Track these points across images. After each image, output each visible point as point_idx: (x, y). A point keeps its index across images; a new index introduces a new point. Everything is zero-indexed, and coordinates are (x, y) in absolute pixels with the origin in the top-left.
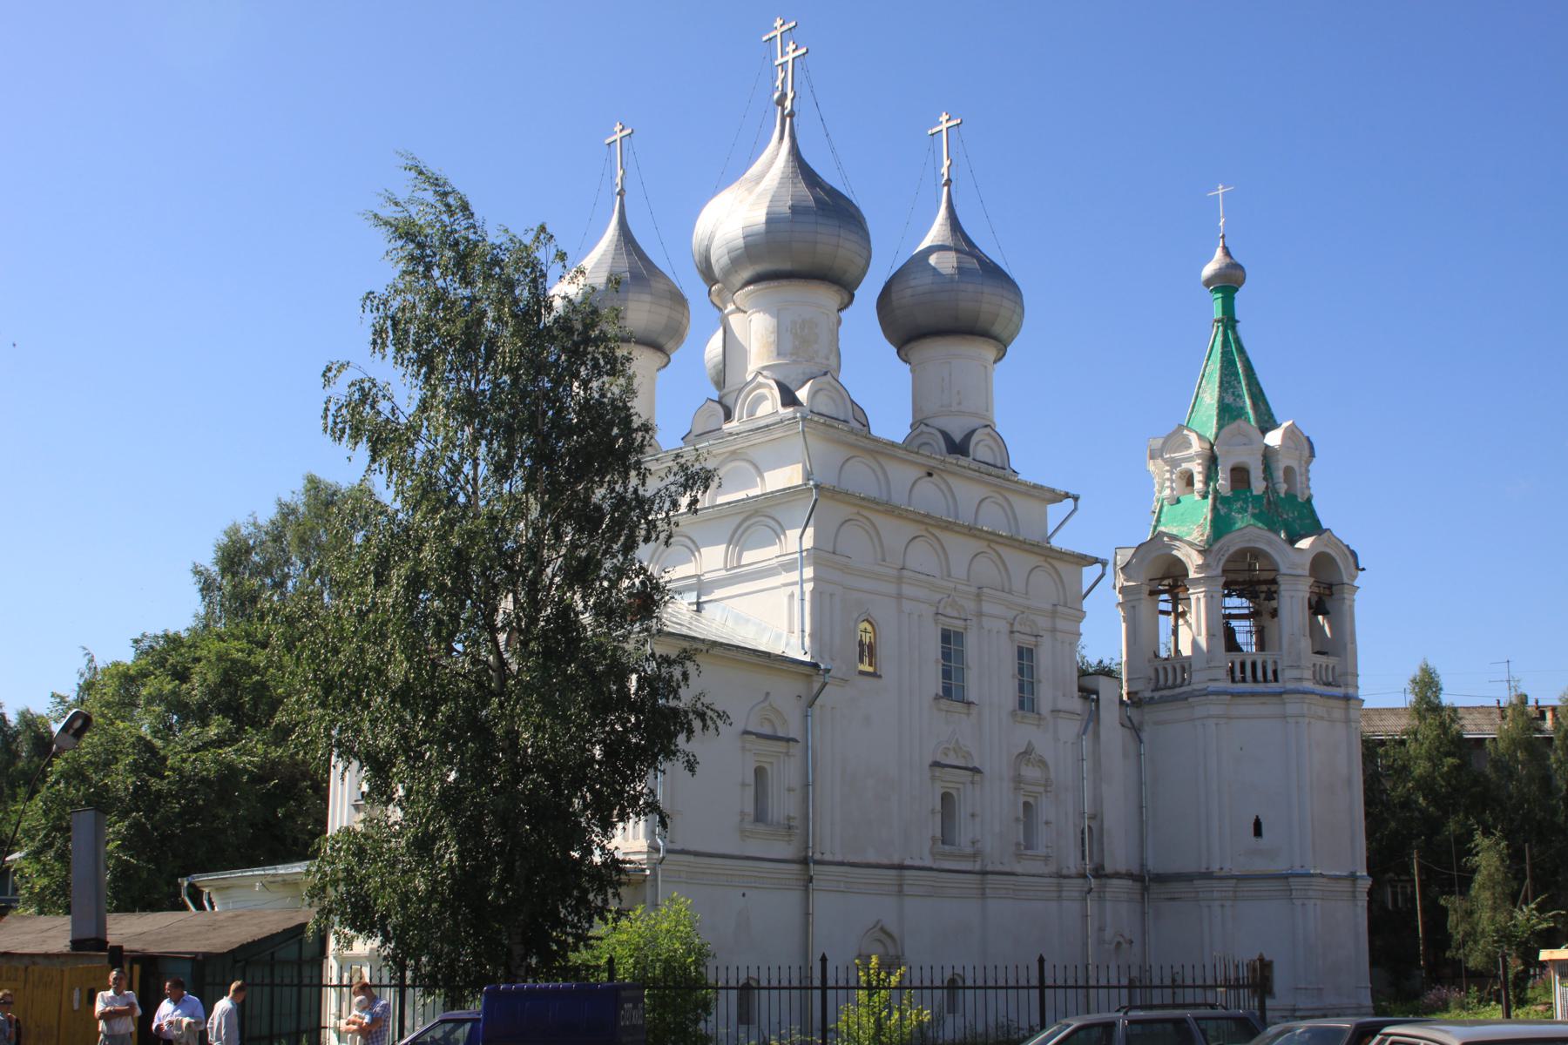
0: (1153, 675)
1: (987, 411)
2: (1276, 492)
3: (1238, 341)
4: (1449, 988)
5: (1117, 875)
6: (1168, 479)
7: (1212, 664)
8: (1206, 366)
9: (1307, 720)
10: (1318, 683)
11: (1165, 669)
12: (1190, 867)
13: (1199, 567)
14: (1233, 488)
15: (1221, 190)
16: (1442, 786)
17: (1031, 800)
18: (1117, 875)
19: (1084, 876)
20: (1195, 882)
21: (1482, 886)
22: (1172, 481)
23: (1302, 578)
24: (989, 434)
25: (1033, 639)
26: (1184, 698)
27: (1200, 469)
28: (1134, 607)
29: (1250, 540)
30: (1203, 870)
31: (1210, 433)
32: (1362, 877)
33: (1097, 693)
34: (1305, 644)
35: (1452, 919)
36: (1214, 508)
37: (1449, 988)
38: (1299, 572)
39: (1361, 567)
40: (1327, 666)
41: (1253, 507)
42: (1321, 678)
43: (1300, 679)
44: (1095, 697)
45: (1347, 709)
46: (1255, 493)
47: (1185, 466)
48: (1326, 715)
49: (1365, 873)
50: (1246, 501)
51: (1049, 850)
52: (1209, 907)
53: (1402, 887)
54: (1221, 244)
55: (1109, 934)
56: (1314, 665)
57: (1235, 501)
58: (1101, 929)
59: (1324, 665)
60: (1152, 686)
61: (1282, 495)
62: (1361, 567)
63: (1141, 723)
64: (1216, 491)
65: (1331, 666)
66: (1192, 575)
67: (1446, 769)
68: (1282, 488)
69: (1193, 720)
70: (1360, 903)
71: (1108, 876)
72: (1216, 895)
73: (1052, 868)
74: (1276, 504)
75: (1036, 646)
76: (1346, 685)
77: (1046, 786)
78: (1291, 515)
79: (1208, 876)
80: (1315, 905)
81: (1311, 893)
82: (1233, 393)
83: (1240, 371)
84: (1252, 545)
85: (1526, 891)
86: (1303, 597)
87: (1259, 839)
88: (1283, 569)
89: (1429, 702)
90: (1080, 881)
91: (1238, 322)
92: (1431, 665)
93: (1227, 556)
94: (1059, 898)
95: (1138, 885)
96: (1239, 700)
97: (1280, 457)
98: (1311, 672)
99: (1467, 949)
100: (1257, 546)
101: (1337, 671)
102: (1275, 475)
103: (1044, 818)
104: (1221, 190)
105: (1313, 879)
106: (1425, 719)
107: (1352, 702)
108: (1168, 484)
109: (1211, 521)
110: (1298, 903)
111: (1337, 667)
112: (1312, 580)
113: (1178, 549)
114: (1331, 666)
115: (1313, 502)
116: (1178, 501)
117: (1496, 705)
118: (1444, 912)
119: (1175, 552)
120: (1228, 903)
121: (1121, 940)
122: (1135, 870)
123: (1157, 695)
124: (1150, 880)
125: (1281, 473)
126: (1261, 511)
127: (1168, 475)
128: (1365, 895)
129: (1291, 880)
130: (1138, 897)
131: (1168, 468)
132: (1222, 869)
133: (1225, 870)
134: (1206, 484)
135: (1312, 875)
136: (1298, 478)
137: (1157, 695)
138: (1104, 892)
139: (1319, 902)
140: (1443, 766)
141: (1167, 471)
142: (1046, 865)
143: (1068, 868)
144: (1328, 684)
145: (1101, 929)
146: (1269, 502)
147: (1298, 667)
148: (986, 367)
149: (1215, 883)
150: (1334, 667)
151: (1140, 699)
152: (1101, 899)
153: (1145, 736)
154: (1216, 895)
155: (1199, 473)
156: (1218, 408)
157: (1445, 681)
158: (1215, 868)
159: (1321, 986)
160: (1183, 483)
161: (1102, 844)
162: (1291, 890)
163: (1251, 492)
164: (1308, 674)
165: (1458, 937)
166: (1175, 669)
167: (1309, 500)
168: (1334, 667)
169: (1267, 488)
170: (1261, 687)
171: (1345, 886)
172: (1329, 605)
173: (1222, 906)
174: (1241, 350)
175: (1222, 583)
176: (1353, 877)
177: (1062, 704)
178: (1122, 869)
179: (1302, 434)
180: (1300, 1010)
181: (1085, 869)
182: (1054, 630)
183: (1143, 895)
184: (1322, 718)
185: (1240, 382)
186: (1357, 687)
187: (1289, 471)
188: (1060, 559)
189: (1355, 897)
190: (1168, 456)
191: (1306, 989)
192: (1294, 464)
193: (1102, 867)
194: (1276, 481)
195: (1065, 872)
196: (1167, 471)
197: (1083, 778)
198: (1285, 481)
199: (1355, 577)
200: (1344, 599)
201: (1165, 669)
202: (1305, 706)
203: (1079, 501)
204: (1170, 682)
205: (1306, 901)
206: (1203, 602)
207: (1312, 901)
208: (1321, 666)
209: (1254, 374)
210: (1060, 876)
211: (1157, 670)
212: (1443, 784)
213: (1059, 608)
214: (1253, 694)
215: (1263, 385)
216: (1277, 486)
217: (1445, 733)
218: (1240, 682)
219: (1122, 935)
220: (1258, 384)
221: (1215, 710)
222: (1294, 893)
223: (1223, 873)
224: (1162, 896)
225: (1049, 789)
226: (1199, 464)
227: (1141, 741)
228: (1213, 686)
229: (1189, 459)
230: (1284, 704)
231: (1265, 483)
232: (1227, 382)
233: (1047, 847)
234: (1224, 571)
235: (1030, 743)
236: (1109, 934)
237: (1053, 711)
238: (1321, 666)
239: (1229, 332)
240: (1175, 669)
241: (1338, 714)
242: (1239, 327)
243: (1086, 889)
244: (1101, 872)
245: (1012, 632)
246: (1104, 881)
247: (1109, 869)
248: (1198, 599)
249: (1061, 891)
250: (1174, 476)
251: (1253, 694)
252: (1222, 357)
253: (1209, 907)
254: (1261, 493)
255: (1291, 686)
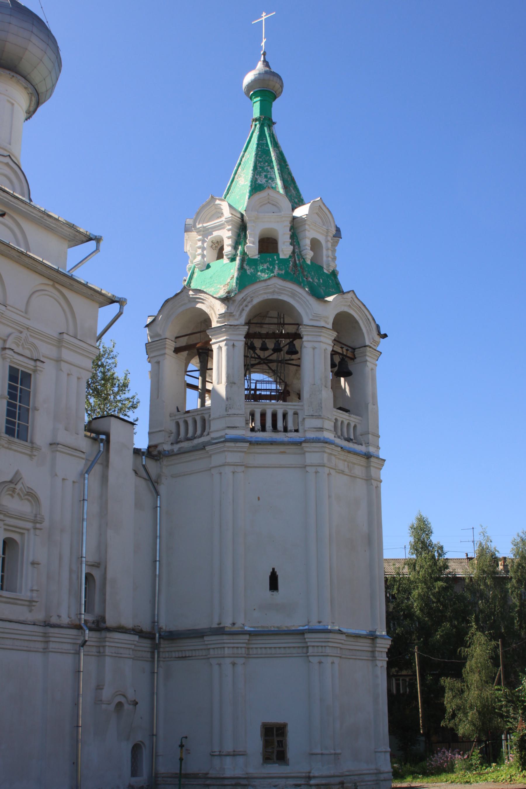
0: (174, 429)
1: (10, 144)
2: (302, 257)
3: (272, 136)
4: (453, 751)
5: (121, 629)
6: (199, 248)
7: (231, 412)
8: (243, 156)
9: (327, 470)
10: (339, 437)
11: (186, 422)
12: (202, 624)
13: (222, 316)
14: (261, 251)
15: (264, 16)
16: (434, 602)
17: (16, 537)
18: (121, 629)
19: (79, 627)
20: (206, 638)
21: (472, 670)
22: (203, 249)
23: (324, 330)
24: (7, 164)
25: (32, 363)
26: (203, 447)
27: (230, 234)
28: (158, 363)
29: (273, 292)
30: (215, 626)
31: (242, 208)
32: (382, 637)
33: (108, 435)
34: (327, 395)
35: (448, 695)
36: (241, 268)
37: (453, 751)
38: (322, 324)
39: (382, 332)
40: (349, 424)
41: (280, 269)
42: (342, 434)
43: (321, 429)
44: (103, 437)
45: (368, 467)
46: (281, 257)
47: (215, 234)
48: (346, 470)
49: (384, 633)
50: (272, 263)
51: (35, 594)
52: (220, 665)
53: (403, 680)
54: (262, 59)
55: (106, 693)
56: (336, 420)
57: (262, 263)
58: (99, 688)
59: (346, 423)
60: (173, 438)
61: (309, 262)
62: (382, 332)
63: (159, 476)
64: (244, 254)
65: (352, 425)
66: (214, 324)
67: (437, 589)
68: (309, 255)
69: (210, 469)
70: (379, 664)
71: (108, 630)
72: (227, 651)
73: (40, 616)
74: (301, 267)
75: (35, 371)
76: (368, 444)
77: (35, 522)
78: (317, 281)
79: (220, 631)
80: (333, 663)
81: (328, 651)
82: (266, 176)
83: (274, 159)
84: (276, 297)
85: (500, 675)
86: (325, 350)
87: (275, 593)
88: (306, 320)
89: (423, 543)
90: (74, 632)
91: (274, 123)
92: (424, 515)
93: (250, 306)
94: (45, 651)
95: (146, 643)
96: (258, 449)
97: (307, 227)
98: (333, 424)
99: (457, 720)
100: (280, 298)
101: (359, 430)
102: (302, 243)
103: (31, 559)
104: (264, 16)
105: (331, 635)
106: (421, 554)
107: (372, 459)
108: (199, 251)
109: (237, 279)
110: (314, 660)
111: (358, 427)
112: (335, 334)
113: (202, 301)
114: (352, 425)
115: (340, 278)
116: (208, 267)
117: (466, 557)
118: (442, 691)
119: (199, 306)
120: (240, 661)
121: (123, 700)
122: (146, 627)
123: (176, 448)
124: (160, 637)
125: (308, 242)
126: (287, 273)
127: (200, 244)
128: (385, 655)
129: (307, 636)
130: (149, 655)
131: (201, 237)
132: (234, 624)
133: (236, 626)
134: (235, 248)
135: (330, 631)
136: (325, 252)
137: (176, 448)
138: (104, 647)
139: (337, 660)
140: (435, 588)
141: (199, 240)
142: (30, 611)
143: (59, 616)
144: (349, 440)
145: (99, 688)
146: (295, 264)
147: (319, 417)
148: (13, 104)
149: (226, 639)
150: (355, 427)
151: (159, 452)
152: (100, 655)
153: (162, 489)
154: (227, 651)
155: (229, 238)
156: (251, 186)
157: (434, 526)
158: (227, 623)
159: (338, 751)
160: (215, 254)
161: (105, 594)
162: (307, 647)
163: (278, 256)
164: (329, 425)
165: (449, 710)
166: (195, 422)
167: (334, 274)
168: (355, 427)
169: (294, 252)
170: (280, 436)
171: (365, 645)
172: (352, 366)
173: (234, 664)
174: (276, 145)
175: (244, 333)
176: (373, 637)
177: (63, 437)
178: (128, 622)
179: (334, 222)
180: (314, 777)
181: (80, 619)
182: (59, 360)
183: (153, 653)
184: (342, 472)
185: (272, 168)
186: (378, 447)
187: (315, 244)
188: (71, 288)
189: (374, 657)
190: (201, 225)
191: (322, 754)
192: (321, 238)
193: (103, 619)
194: (302, 248)
195: (54, 620)
196: (199, 240)
197: (83, 519)
198: (312, 249)
199: (378, 344)
200: (366, 361)
201: (186, 422)
202: (326, 455)
203: (102, 243)
204: (190, 434)
205: (323, 659)
206: (224, 349)
207: (330, 660)
208: (342, 422)
209: (287, 165)
210: (47, 624)
211: (178, 424)
212: (434, 600)
213: (65, 336)
214: (272, 443)
215: (294, 175)
216: (303, 253)
217: (435, 564)
218: (259, 430)
219: (124, 696)
220: (290, 174)
221: (231, 458)
222: (310, 650)
223: (235, 629)
224: (174, 655)
225: (38, 526)
226: (229, 230)
227: (158, 494)
228: (232, 433)
229: (220, 227)
230: (304, 453)
231: (292, 247)
232: (260, 167)
233: (32, 590)
234: (248, 323)
235: (17, 473)
236: (106, 693)
237: (51, 444)
238: (342, 422)
239: (266, 129)
240: (195, 422)
241: (359, 471)
242: (276, 129)
243: (80, 642)
244: (102, 625)
245: (4, 349)
246: (104, 634)
247: (110, 622)
248: (220, 348)
249: (47, 642)
250: (205, 245)
251: (272, 443)
252: (257, 147)
253: (220, 665)
254: (288, 257)
255: (311, 435)
